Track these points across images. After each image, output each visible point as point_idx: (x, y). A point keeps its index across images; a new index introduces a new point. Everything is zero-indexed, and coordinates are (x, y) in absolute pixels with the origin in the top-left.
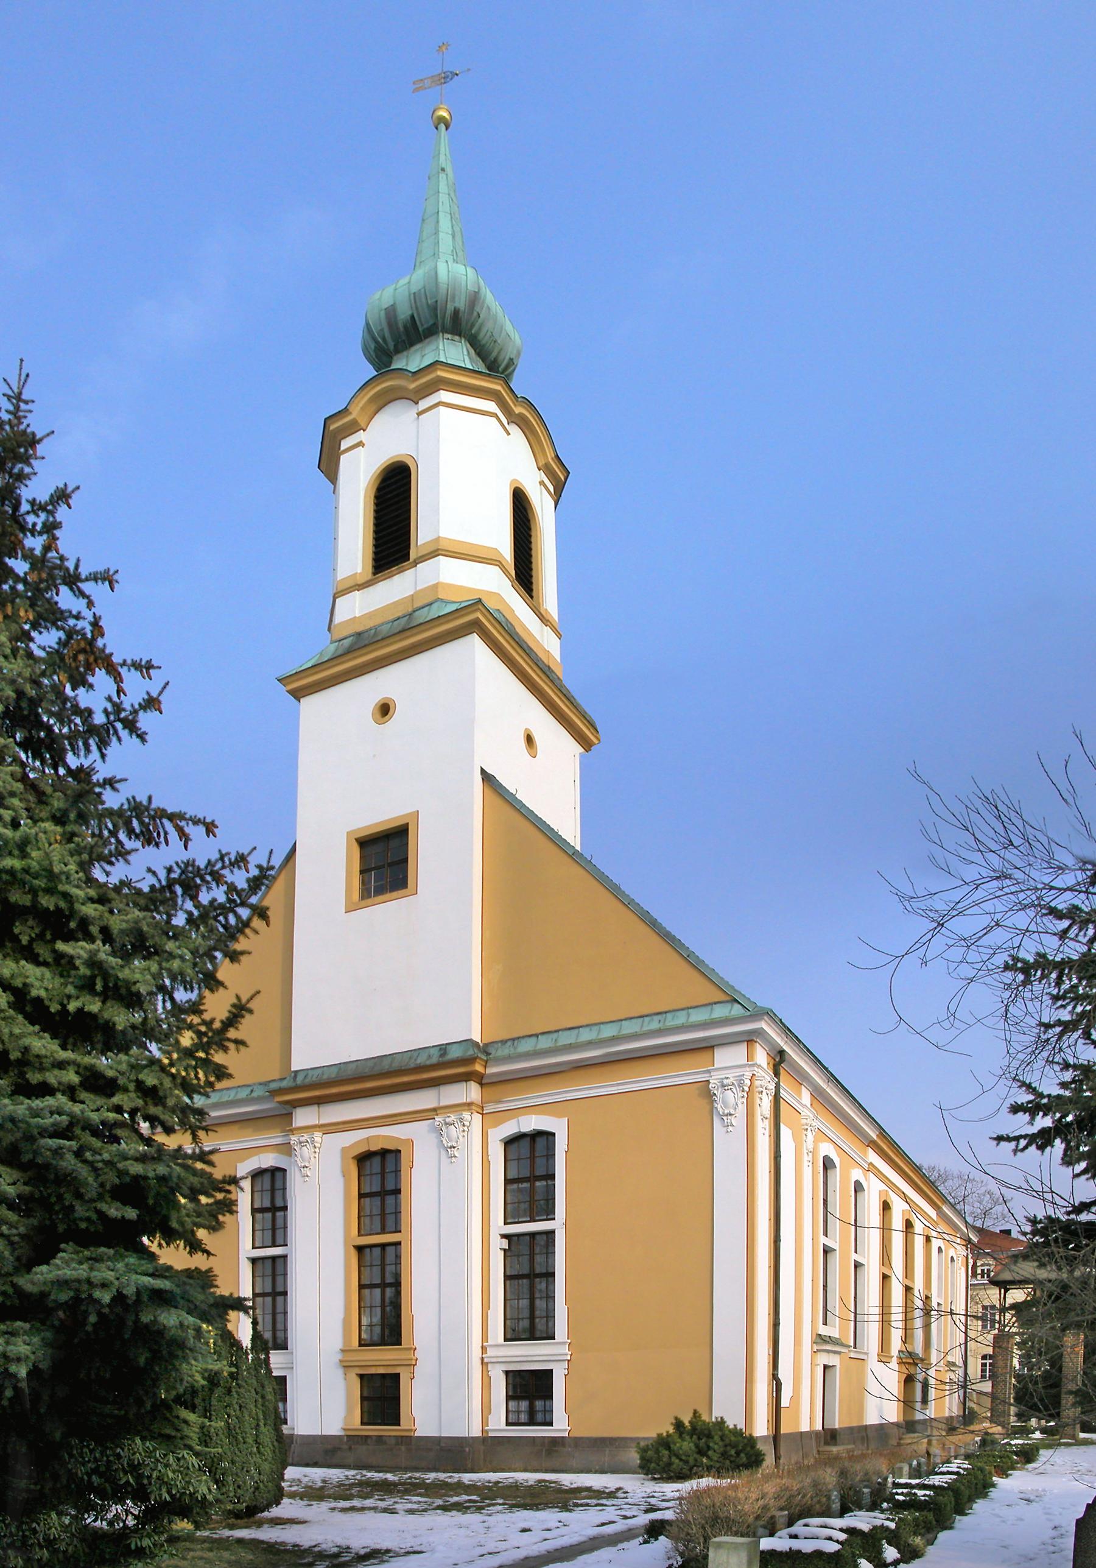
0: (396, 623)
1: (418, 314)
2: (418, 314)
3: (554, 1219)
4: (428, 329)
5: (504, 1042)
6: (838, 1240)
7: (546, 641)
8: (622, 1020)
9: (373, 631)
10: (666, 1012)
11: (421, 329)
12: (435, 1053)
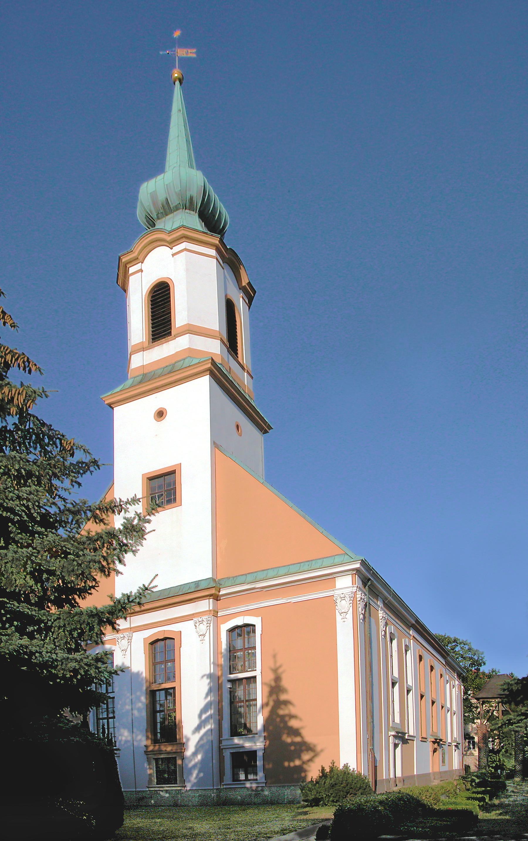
0: (165, 369)
1: (170, 197)
2: (170, 197)
3: (256, 670)
4: (176, 206)
5: (228, 578)
6: (154, 294)
7: (179, 88)
8: (289, 565)
9: (153, 373)
10: (312, 561)
11: (171, 206)
12: (193, 586)
